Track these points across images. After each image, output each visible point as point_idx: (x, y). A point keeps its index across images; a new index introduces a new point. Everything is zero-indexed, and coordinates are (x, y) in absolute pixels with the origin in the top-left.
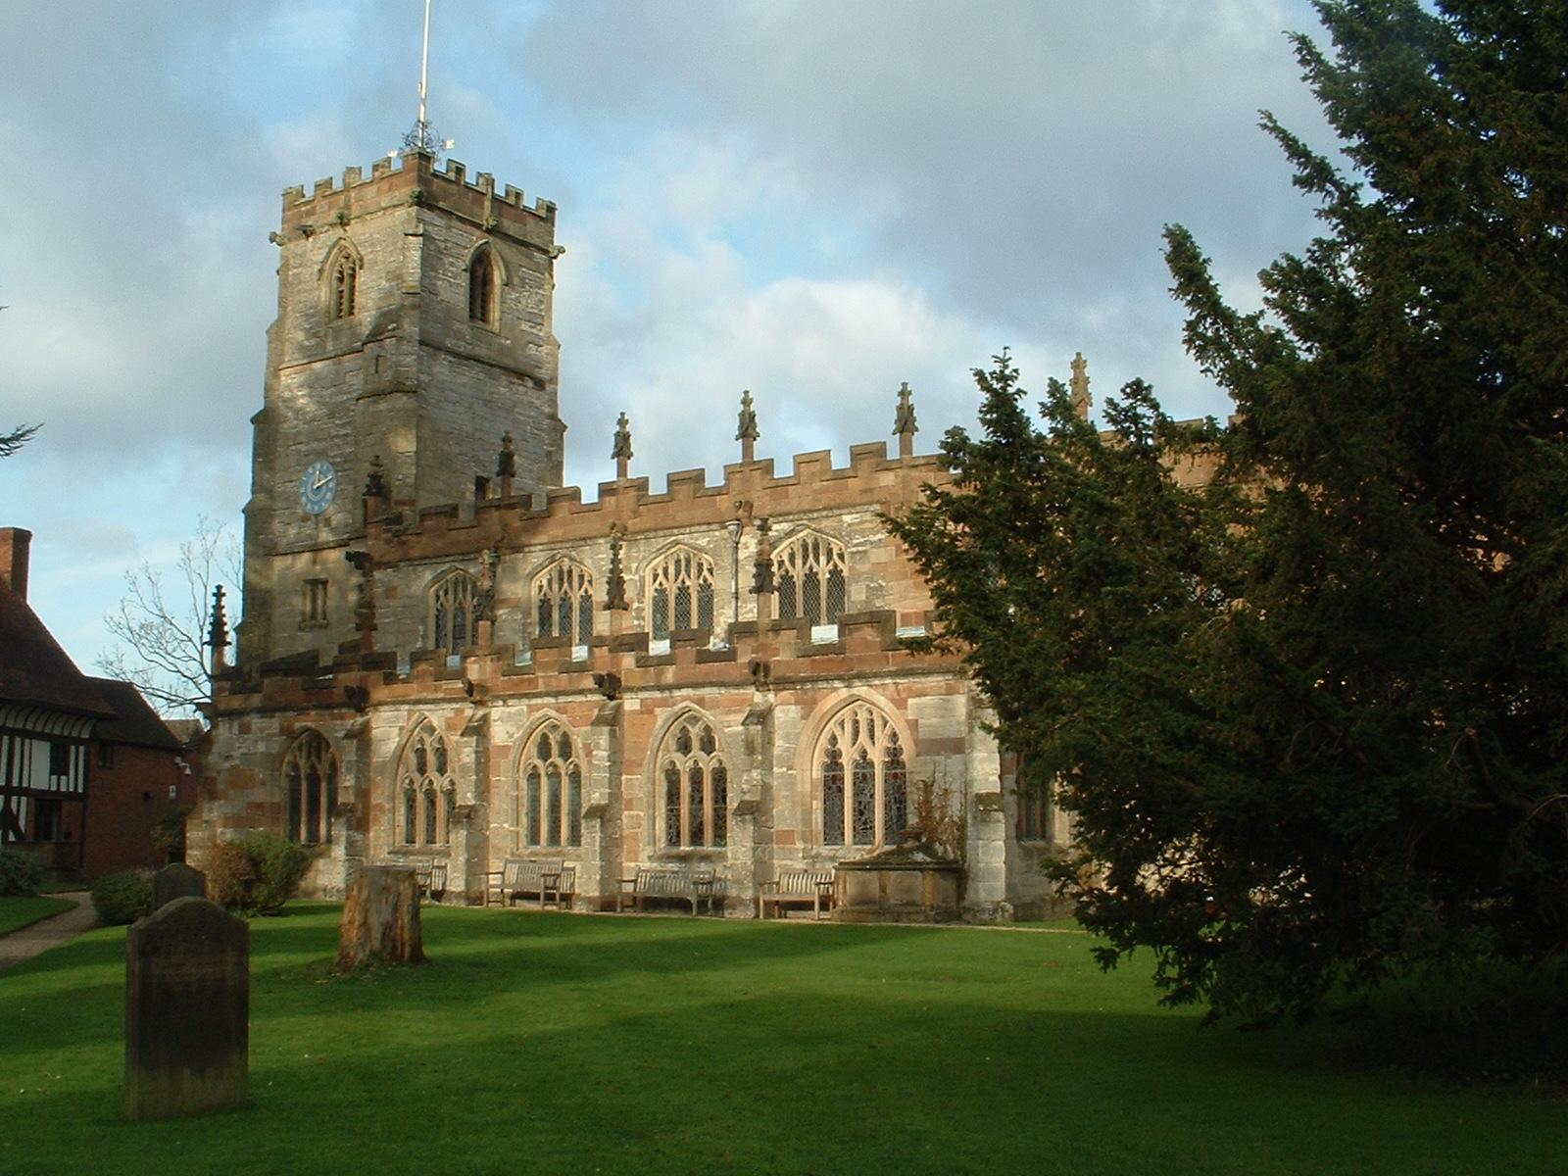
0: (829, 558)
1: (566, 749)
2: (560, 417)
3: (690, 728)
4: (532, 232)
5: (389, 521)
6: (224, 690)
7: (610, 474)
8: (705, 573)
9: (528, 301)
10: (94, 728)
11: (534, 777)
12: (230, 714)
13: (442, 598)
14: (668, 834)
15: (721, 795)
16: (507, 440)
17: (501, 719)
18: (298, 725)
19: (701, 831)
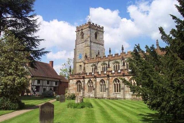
4: (102, 30)
9: (101, 37)
16: (99, 51)
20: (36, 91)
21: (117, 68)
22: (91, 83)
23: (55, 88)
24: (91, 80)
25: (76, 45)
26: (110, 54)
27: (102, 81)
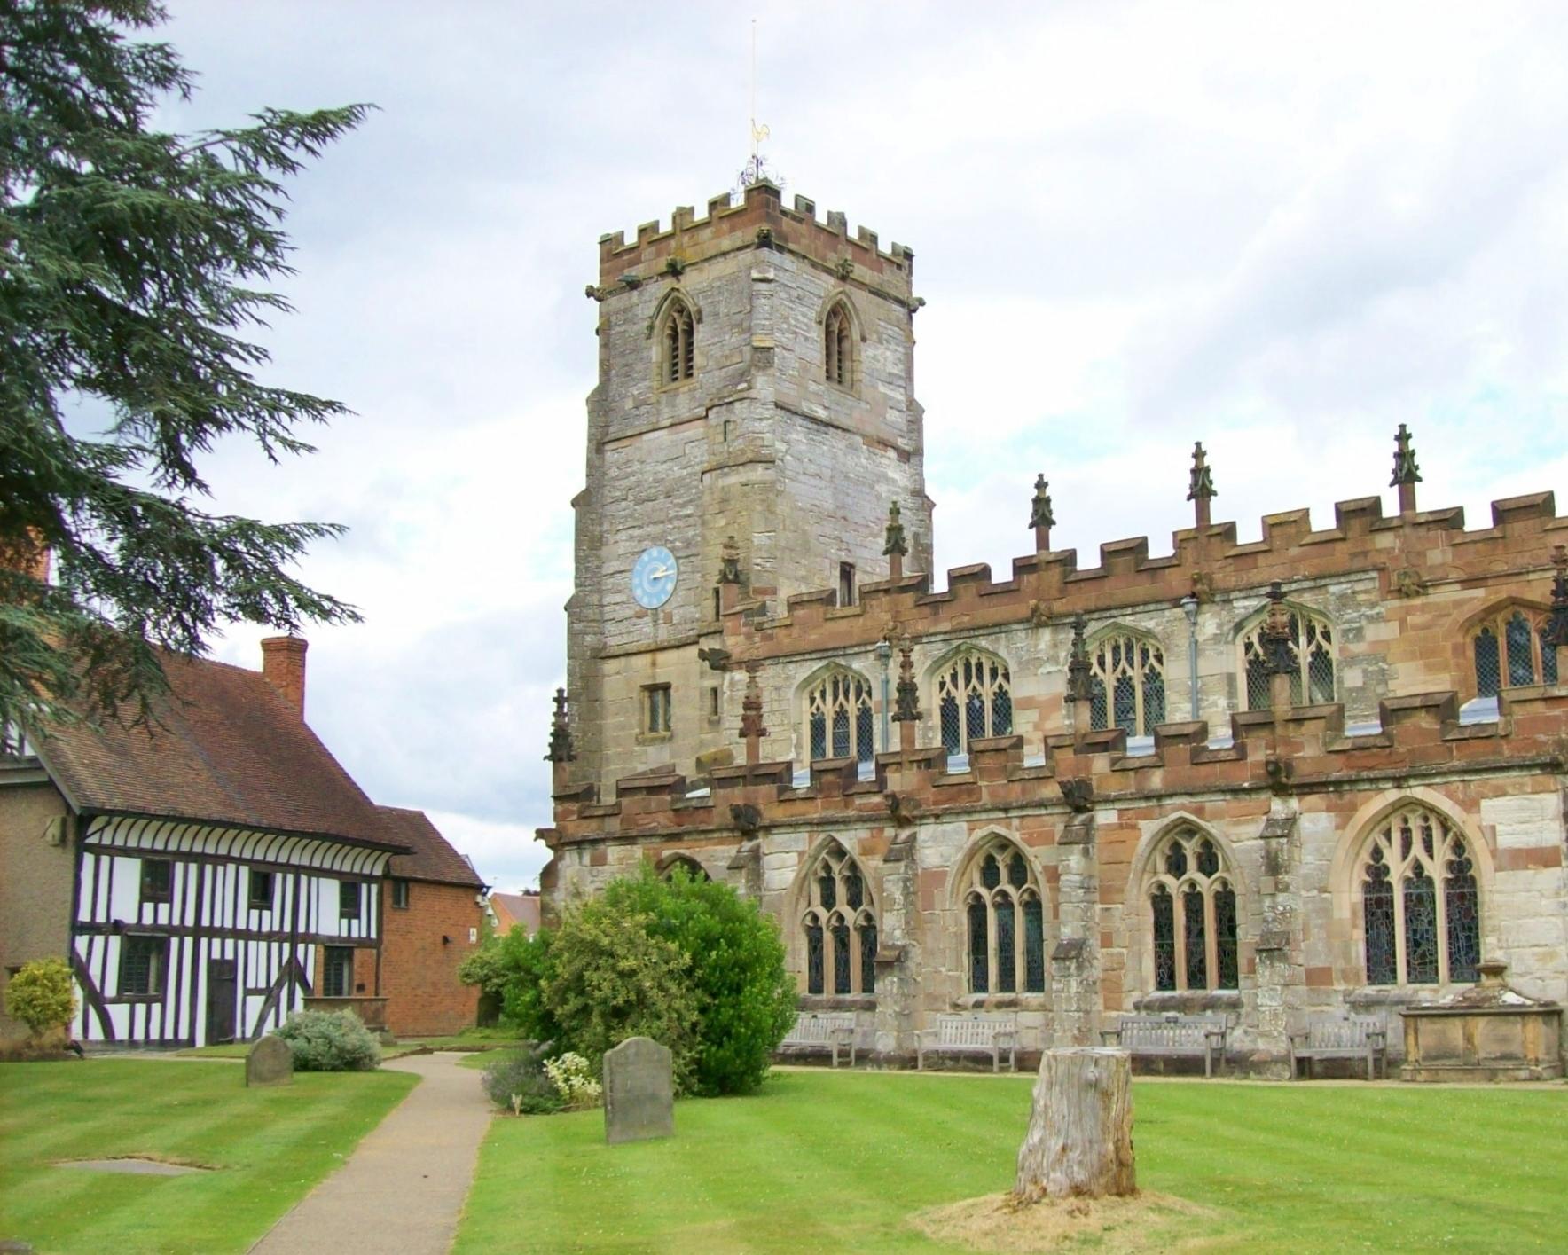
0: (1310, 640)
1: (1019, 870)
2: (927, 492)
3: (1184, 843)
5: (748, 613)
6: (572, 813)
7: (1028, 548)
8: (1152, 660)
10: (387, 864)
11: (977, 910)
12: (579, 844)
13: (818, 701)
14: (1158, 975)
15: (1227, 926)
17: (934, 839)
18: (666, 853)
19: (1203, 971)
20: (1268, 844)
21: (841, 742)
22: (841, 891)
23: (337, 953)
24: (840, 853)
25: (599, 444)
26: (1043, 542)
27: (1001, 864)
